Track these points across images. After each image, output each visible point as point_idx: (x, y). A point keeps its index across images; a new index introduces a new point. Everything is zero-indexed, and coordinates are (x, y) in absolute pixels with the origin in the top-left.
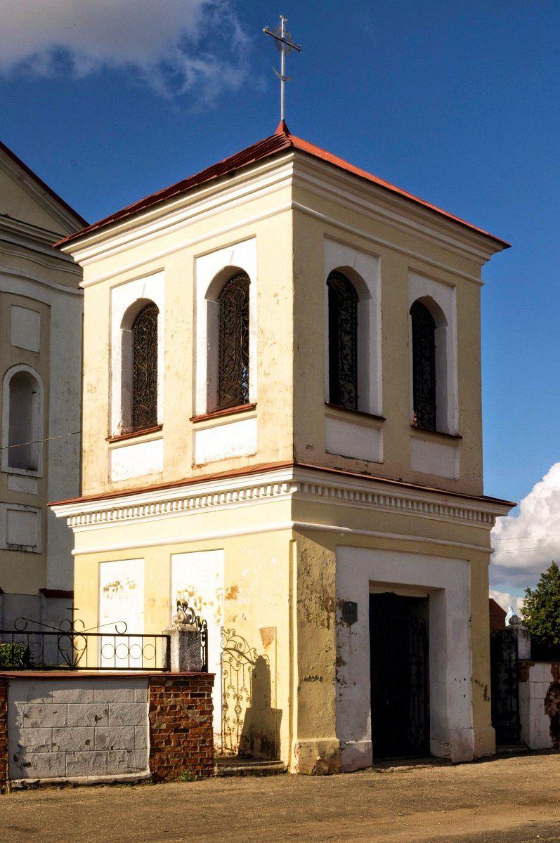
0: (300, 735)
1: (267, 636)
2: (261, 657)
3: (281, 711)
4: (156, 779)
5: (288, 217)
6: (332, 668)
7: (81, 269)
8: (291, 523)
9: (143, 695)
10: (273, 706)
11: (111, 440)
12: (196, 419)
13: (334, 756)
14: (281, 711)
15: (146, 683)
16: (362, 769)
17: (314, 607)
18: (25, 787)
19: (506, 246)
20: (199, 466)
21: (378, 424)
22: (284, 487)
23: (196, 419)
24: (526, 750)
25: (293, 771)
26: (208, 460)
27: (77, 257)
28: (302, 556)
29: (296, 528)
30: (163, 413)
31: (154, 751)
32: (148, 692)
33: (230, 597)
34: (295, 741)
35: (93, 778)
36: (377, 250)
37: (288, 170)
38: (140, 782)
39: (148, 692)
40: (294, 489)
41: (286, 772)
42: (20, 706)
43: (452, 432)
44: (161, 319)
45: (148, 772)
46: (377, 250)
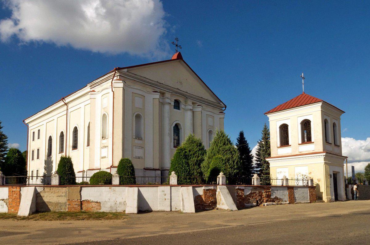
0: (327, 196)
1: (319, 180)
2: (318, 184)
3: (323, 192)
4: (310, 202)
5: (320, 111)
6: (330, 185)
7: (269, 118)
8: (324, 162)
9: (307, 190)
10: (321, 191)
11: (278, 147)
12: (299, 144)
13: (331, 199)
14: (323, 192)
15: (287, 188)
16: (334, 202)
17: (327, 175)
18: (297, 203)
19: (345, 112)
20: (300, 152)
21: (331, 145)
22: (323, 156)
23: (299, 144)
24: (349, 200)
25: (326, 202)
26: (302, 151)
27: (268, 116)
28: (325, 167)
29: (325, 163)
30: (290, 142)
31: (310, 198)
32: (308, 189)
33: (309, 174)
34: (326, 197)
35: (304, 202)
36: (329, 115)
37: (321, 104)
38: (309, 203)
39: (308, 189)
40: (324, 156)
41: (324, 202)
42: (295, 191)
43: (338, 145)
44: (289, 128)
45: (309, 201)
46: (329, 115)
